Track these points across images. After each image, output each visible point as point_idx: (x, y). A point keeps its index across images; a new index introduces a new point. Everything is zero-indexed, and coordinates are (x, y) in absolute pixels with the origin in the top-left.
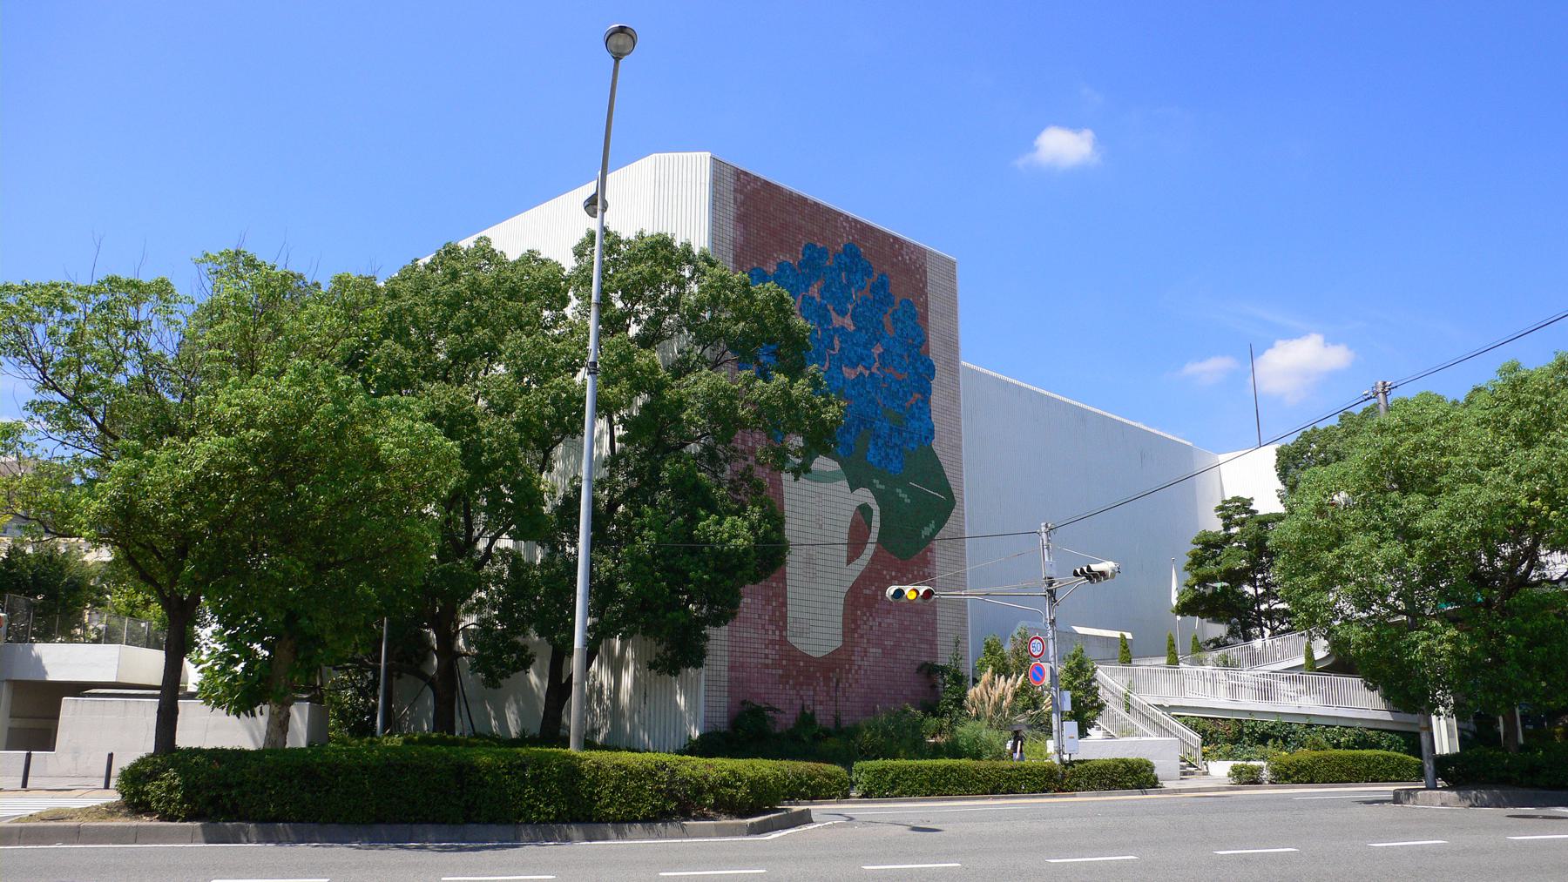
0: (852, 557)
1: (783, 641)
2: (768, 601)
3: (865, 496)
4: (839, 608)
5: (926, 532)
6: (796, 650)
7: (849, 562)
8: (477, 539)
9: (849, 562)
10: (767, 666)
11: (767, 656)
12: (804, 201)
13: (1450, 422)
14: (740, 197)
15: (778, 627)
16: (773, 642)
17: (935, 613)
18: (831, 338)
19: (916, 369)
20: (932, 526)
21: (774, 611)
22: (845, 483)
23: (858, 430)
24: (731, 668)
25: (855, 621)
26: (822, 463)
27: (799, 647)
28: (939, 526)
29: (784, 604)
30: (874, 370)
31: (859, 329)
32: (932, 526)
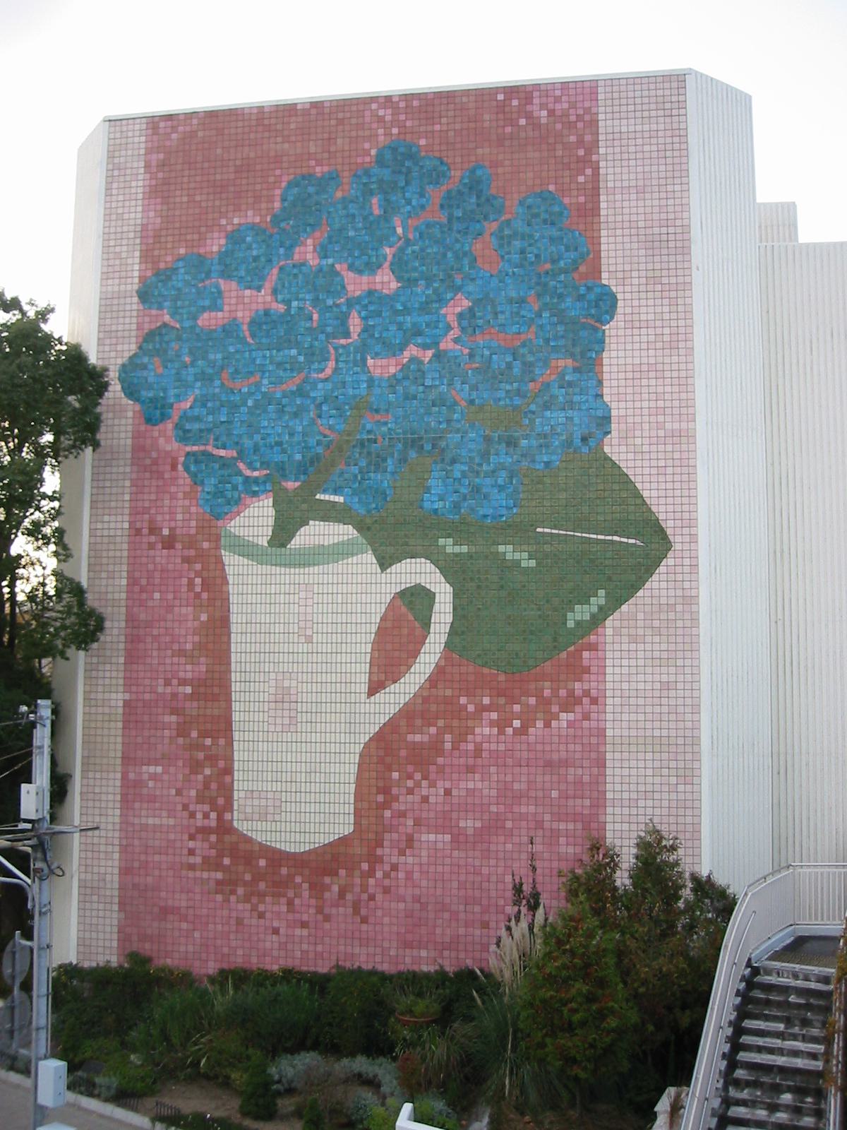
0: (386, 669)
1: (224, 828)
2: (196, 767)
3: (417, 571)
4: (350, 770)
5: (581, 613)
6: (249, 840)
7: (372, 692)
8: (613, 1030)
9: (372, 692)
10: (192, 867)
11: (191, 852)
12: (287, 111)
13: (252, 972)
14: (157, 157)
15: (214, 806)
16: (205, 831)
17: (601, 763)
18: (343, 319)
19: (560, 315)
20: (600, 599)
21: (206, 785)
22: (369, 558)
23: (403, 460)
24: (125, 871)
25: (386, 791)
26: (315, 533)
27: (259, 837)
28: (616, 602)
29: (229, 771)
30: (447, 344)
31: (410, 283)
32: (600, 599)
